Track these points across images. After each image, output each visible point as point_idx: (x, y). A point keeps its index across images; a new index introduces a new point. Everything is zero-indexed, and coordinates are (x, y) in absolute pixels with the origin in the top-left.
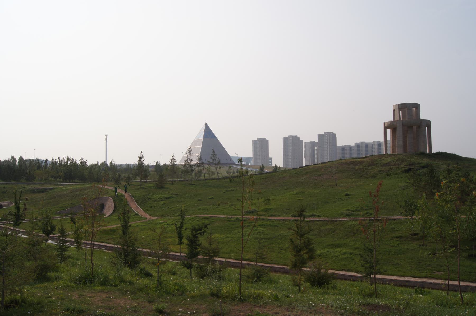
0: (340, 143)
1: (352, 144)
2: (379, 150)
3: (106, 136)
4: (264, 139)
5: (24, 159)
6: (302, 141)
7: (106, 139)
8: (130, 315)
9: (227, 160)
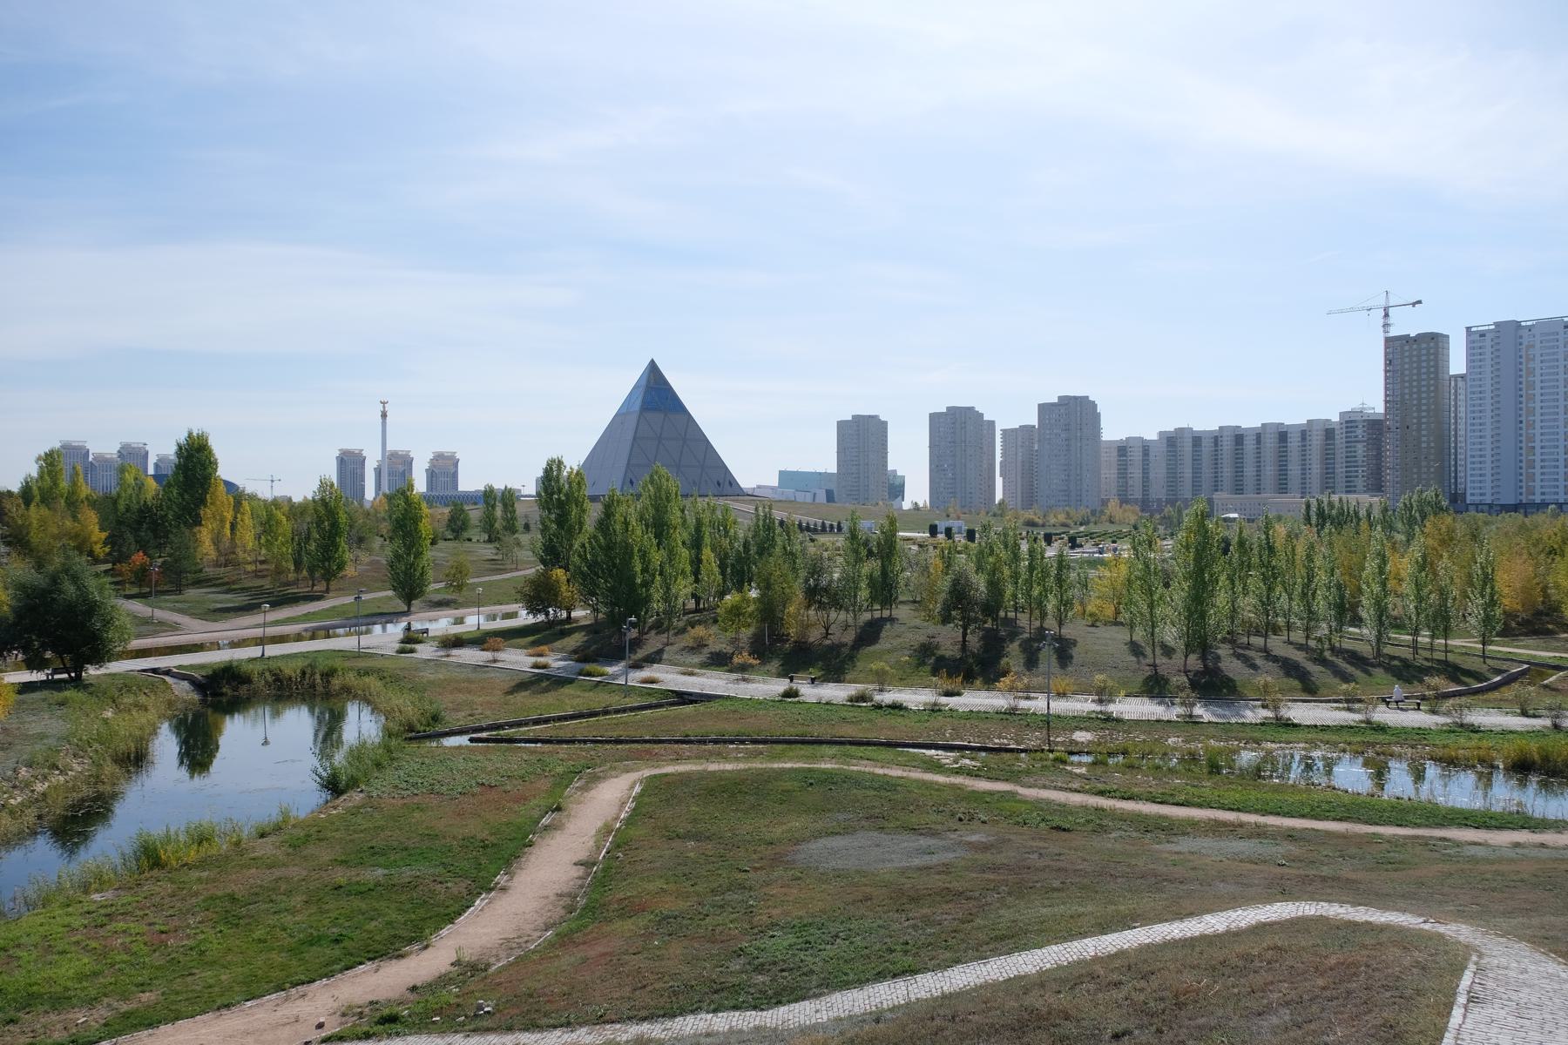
0: (1113, 430)
1: (1151, 435)
2: (1327, 454)
3: (384, 403)
4: (873, 419)
5: (890, 468)
6: (992, 424)
7: (384, 415)
8: (767, 1043)
9: (719, 484)
